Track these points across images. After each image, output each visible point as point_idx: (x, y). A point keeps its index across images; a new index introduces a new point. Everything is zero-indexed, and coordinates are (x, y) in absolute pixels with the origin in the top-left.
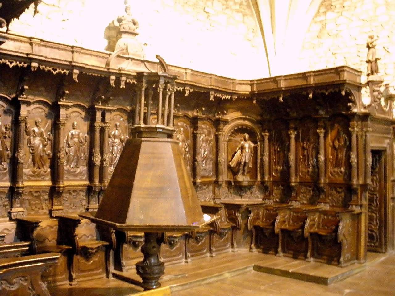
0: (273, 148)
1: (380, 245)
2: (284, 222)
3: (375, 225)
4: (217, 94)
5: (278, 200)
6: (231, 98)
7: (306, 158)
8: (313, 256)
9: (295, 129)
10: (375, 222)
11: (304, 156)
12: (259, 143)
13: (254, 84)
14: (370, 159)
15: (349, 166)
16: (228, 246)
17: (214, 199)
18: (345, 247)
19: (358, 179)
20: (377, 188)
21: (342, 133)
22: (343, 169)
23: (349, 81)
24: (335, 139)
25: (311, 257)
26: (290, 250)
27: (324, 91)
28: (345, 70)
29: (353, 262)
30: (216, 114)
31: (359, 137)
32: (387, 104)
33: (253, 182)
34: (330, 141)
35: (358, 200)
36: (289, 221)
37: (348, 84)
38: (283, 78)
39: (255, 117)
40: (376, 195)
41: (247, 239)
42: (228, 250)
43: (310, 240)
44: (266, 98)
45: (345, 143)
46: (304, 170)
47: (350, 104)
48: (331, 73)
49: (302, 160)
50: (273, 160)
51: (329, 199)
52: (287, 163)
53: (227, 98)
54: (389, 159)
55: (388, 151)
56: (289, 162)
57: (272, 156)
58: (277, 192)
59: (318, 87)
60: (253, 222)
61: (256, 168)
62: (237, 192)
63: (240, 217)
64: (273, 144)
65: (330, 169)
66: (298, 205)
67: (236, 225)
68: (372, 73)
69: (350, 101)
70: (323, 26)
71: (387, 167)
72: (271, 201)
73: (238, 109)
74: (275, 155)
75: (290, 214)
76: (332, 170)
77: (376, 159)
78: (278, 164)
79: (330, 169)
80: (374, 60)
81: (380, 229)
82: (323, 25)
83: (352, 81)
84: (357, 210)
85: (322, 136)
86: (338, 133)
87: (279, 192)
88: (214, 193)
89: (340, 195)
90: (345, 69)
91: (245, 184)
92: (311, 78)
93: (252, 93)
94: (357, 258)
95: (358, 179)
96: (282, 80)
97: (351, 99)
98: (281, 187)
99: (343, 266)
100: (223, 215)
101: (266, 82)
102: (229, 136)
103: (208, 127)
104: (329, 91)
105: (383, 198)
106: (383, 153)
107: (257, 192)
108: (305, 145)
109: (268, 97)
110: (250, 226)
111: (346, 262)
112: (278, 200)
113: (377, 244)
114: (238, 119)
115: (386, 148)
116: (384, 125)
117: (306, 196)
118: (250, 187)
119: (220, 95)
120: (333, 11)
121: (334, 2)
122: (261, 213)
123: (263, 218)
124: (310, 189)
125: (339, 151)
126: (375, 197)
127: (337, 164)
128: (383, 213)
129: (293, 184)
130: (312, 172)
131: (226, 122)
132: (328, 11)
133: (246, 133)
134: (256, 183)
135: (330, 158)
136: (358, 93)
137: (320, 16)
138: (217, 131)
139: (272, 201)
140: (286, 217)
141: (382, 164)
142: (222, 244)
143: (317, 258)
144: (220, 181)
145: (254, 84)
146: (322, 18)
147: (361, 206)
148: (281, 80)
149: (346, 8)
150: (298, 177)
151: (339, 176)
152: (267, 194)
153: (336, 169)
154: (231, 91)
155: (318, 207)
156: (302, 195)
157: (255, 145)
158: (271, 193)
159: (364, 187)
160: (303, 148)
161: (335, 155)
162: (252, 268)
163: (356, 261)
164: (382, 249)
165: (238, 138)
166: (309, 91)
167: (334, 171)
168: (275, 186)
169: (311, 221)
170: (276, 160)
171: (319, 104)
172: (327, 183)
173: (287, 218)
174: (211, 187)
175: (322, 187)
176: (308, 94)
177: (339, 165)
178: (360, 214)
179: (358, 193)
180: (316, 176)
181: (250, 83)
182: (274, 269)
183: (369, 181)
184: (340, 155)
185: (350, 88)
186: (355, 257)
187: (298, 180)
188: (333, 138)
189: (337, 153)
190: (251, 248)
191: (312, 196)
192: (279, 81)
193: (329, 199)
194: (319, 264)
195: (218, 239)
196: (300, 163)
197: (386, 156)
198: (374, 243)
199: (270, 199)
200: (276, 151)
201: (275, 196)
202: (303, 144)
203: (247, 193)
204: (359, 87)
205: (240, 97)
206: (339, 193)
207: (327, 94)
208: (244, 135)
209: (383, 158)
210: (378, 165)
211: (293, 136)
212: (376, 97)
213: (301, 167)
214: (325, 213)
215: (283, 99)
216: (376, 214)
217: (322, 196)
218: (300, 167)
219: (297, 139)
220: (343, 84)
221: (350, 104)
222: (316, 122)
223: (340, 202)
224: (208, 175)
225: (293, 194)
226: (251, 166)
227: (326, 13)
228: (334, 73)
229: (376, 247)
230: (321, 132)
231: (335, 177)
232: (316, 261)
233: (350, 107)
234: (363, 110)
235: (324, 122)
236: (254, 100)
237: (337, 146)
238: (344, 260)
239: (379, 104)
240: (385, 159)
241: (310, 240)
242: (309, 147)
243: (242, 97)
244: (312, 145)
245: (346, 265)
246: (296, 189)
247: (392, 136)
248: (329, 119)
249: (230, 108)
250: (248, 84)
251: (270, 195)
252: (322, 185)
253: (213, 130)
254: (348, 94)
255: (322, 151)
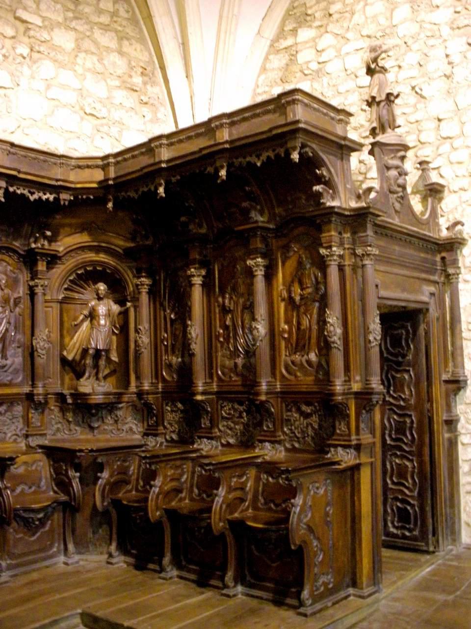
0: (162, 313)
1: (424, 536)
2: (178, 491)
3: (411, 486)
4: (15, 188)
5: (175, 437)
6: (57, 200)
7: (230, 332)
8: (240, 579)
9: (204, 264)
10: (410, 481)
11: (226, 328)
12: (129, 304)
13: (108, 164)
14: (375, 326)
15: (325, 347)
16: (55, 549)
17: (27, 436)
18: (317, 556)
19: (348, 381)
20: (412, 402)
21: (308, 266)
22: (313, 356)
23: (306, 123)
24: (292, 282)
25: (236, 583)
26: (190, 562)
27: (252, 159)
28: (298, 100)
29: (342, 594)
30: (32, 240)
31: (348, 270)
32: (426, 209)
33: (115, 394)
34: (281, 287)
35: (349, 435)
36: (191, 491)
37: (305, 131)
38: (164, 141)
39: (120, 243)
40: (410, 416)
41: (100, 531)
42: (55, 560)
43: (230, 540)
44: (132, 194)
45: (317, 289)
46: (227, 363)
47: (318, 188)
48: (268, 112)
49: (222, 339)
50: (162, 341)
51: (284, 433)
52: (183, 345)
53: (44, 197)
54: (435, 330)
55: (433, 313)
56: (189, 345)
57: (161, 333)
58: (172, 416)
59: (238, 148)
60: (111, 490)
61: (127, 362)
62: (83, 418)
63: (77, 480)
64: (162, 305)
65: (284, 356)
66: (217, 447)
67: (70, 499)
68: (383, 129)
69: (319, 180)
70: (293, 58)
71: (432, 347)
72: (160, 439)
73: (82, 228)
74: (166, 331)
75: (193, 473)
76: (288, 359)
77: (408, 332)
78: (173, 352)
79: (284, 356)
80: (384, 97)
81: (421, 496)
82: (293, 55)
83: (313, 126)
84: (345, 458)
85: (260, 273)
86: (300, 264)
87: (177, 416)
88: (27, 422)
89: (309, 420)
90: (298, 97)
91: (98, 399)
92: (223, 132)
93: (103, 184)
94: (354, 584)
95: (348, 381)
96: (164, 144)
97: (323, 176)
98: (180, 405)
99: (309, 611)
100: (43, 475)
101: (133, 157)
102: (66, 289)
103: (9, 268)
104: (264, 157)
105: (427, 421)
106: (421, 317)
107: (129, 419)
108: (227, 301)
109: (136, 191)
110: (103, 501)
111: (316, 599)
112: (175, 437)
113: (416, 533)
114: (82, 248)
115: (427, 303)
116: (420, 250)
117: (232, 425)
118: (110, 407)
119: (26, 192)
120: (310, 26)
121: (311, 7)
122: (132, 468)
123: (137, 480)
124: (241, 408)
125: (302, 309)
126: (408, 420)
127: (300, 345)
128: (427, 458)
129: (199, 398)
130: (244, 366)
131: (53, 260)
132: (300, 27)
133: (100, 281)
134: (126, 398)
135: (284, 331)
136: (339, 162)
137: (286, 38)
138: (32, 279)
139: (164, 440)
140: (183, 479)
141: (420, 342)
142: (36, 547)
143: (251, 586)
144: (39, 395)
145: (108, 164)
146: (290, 41)
147: (358, 448)
148: (161, 145)
149: (335, 16)
150: (215, 379)
151: (306, 373)
152: (151, 422)
153: (297, 357)
154: (53, 183)
155: (257, 452)
156: (225, 423)
157: (123, 309)
158: (160, 421)
159: (364, 398)
160: (225, 311)
161: (294, 320)
162: (77, 620)
163: (351, 590)
164: (427, 544)
165: (87, 295)
166: (218, 164)
167: (293, 362)
168: (167, 405)
169: (230, 490)
170: (170, 342)
171: (249, 197)
172: (277, 393)
173: (186, 481)
174: (19, 409)
175: (262, 402)
176: (217, 171)
177: (304, 346)
178: (356, 468)
179: (348, 416)
180: (249, 377)
181: (100, 163)
182: (122, 625)
183: (376, 384)
184: (305, 322)
185: (314, 146)
186: (347, 580)
187: (215, 387)
188: (289, 279)
189: (298, 316)
190: (111, 555)
191: (246, 426)
192: (157, 150)
193: (284, 433)
194: (254, 603)
195: (21, 535)
196: (219, 345)
197: (428, 324)
198: (410, 530)
199: (156, 435)
200: (168, 320)
201: (168, 426)
202: (224, 298)
203: (106, 421)
204: (345, 148)
205: (80, 197)
206: (307, 416)
207: (259, 164)
208: (96, 286)
209: (422, 327)
210: (412, 346)
211: (197, 281)
212: (392, 182)
213: (222, 358)
214: (270, 468)
215: (166, 191)
216: (412, 461)
217: (268, 425)
218: (220, 354)
219: (207, 286)
220: (293, 131)
221: (318, 188)
222: (244, 239)
223: (309, 439)
224: (10, 381)
225: (205, 422)
226: (114, 357)
227: (297, 31)
228: (274, 111)
229: (415, 539)
230: (258, 264)
231: (296, 376)
232: (248, 595)
233: (319, 195)
234: (354, 204)
235: (264, 239)
236: (110, 200)
237: (297, 298)
238: (312, 594)
239: (402, 198)
240: (427, 333)
241: (230, 540)
242: (236, 303)
243: (84, 197)
244: (241, 301)
245: (318, 606)
246: (209, 409)
247: (440, 277)
248: (279, 232)
249: (63, 226)
250: (97, 167)
251: (157, 424)
252: (263, 398)
253: (24, 276)
254: (311, 163)
255: (261, 310)
